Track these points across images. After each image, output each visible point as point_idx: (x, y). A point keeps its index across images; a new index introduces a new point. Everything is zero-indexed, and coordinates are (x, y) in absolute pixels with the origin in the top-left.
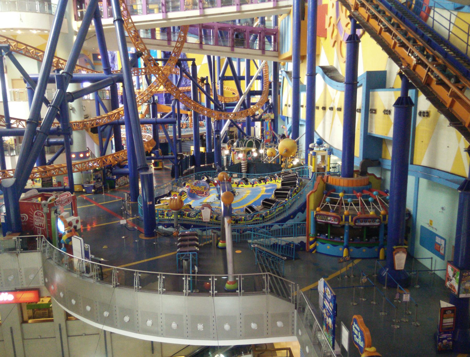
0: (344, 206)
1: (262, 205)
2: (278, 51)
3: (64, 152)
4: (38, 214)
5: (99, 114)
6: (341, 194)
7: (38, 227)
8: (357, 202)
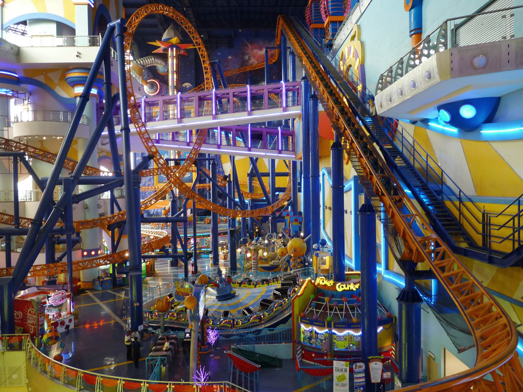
0: (328, 312)
1: (260, 306)
2: (294, 151)
3: (44, 252)
4: (31, 312)
5: (112, 211)
6: (326, 299)
7: (30, 326)
8: (342, 308)
